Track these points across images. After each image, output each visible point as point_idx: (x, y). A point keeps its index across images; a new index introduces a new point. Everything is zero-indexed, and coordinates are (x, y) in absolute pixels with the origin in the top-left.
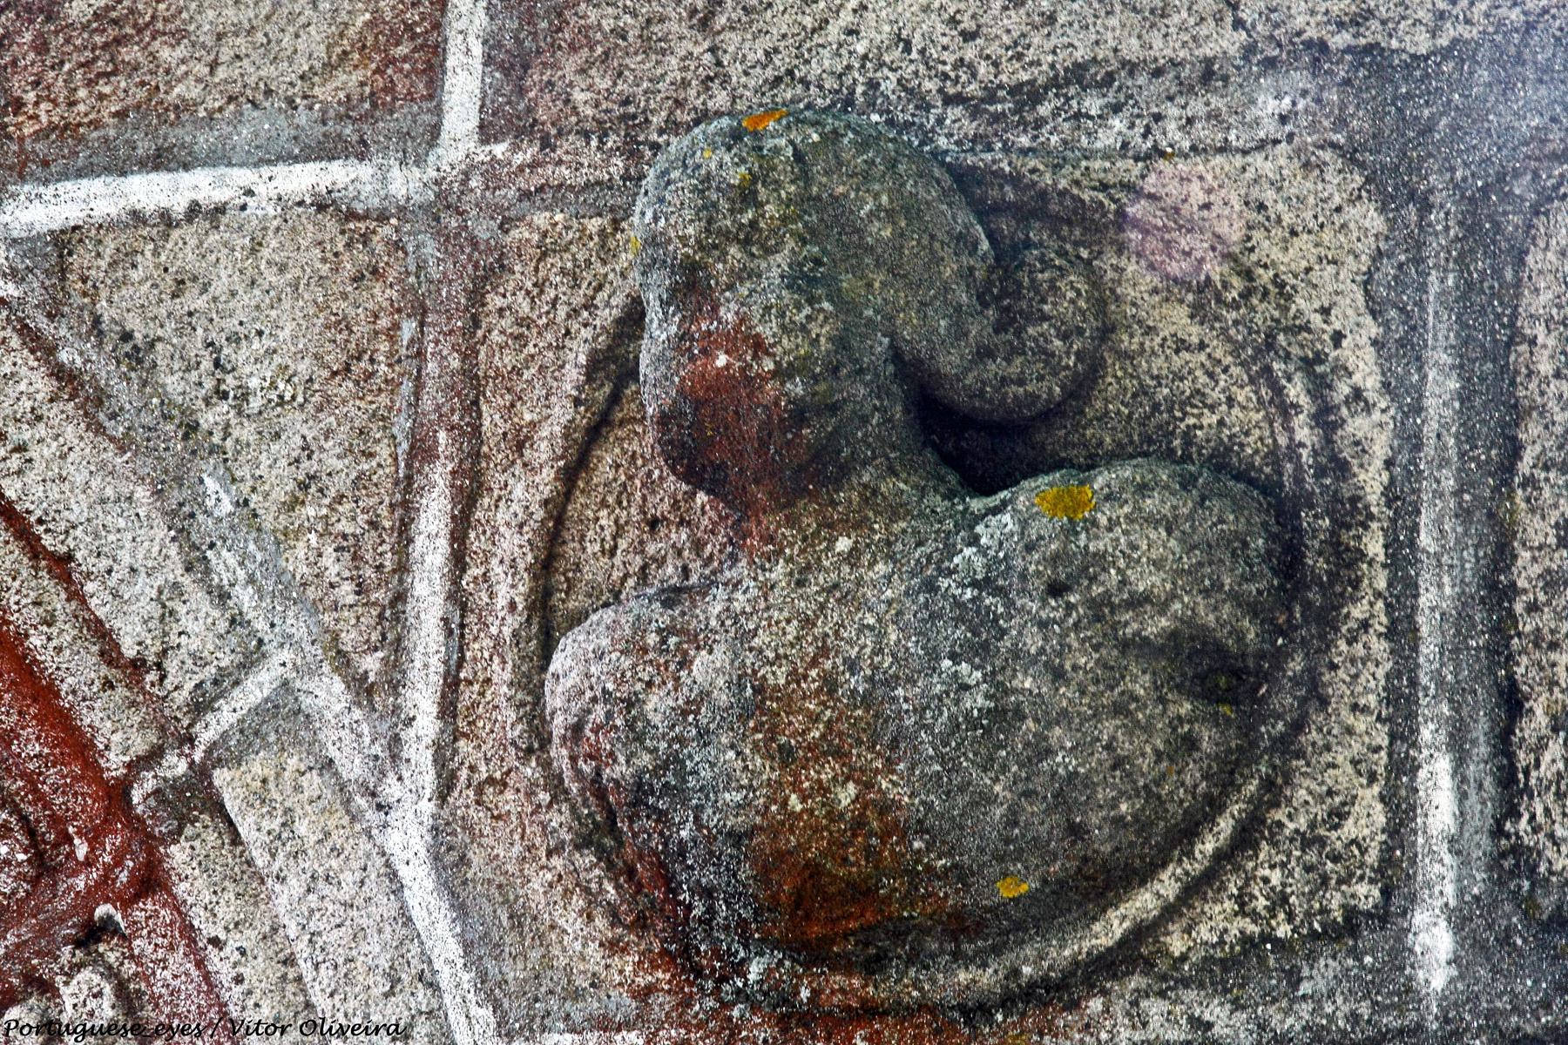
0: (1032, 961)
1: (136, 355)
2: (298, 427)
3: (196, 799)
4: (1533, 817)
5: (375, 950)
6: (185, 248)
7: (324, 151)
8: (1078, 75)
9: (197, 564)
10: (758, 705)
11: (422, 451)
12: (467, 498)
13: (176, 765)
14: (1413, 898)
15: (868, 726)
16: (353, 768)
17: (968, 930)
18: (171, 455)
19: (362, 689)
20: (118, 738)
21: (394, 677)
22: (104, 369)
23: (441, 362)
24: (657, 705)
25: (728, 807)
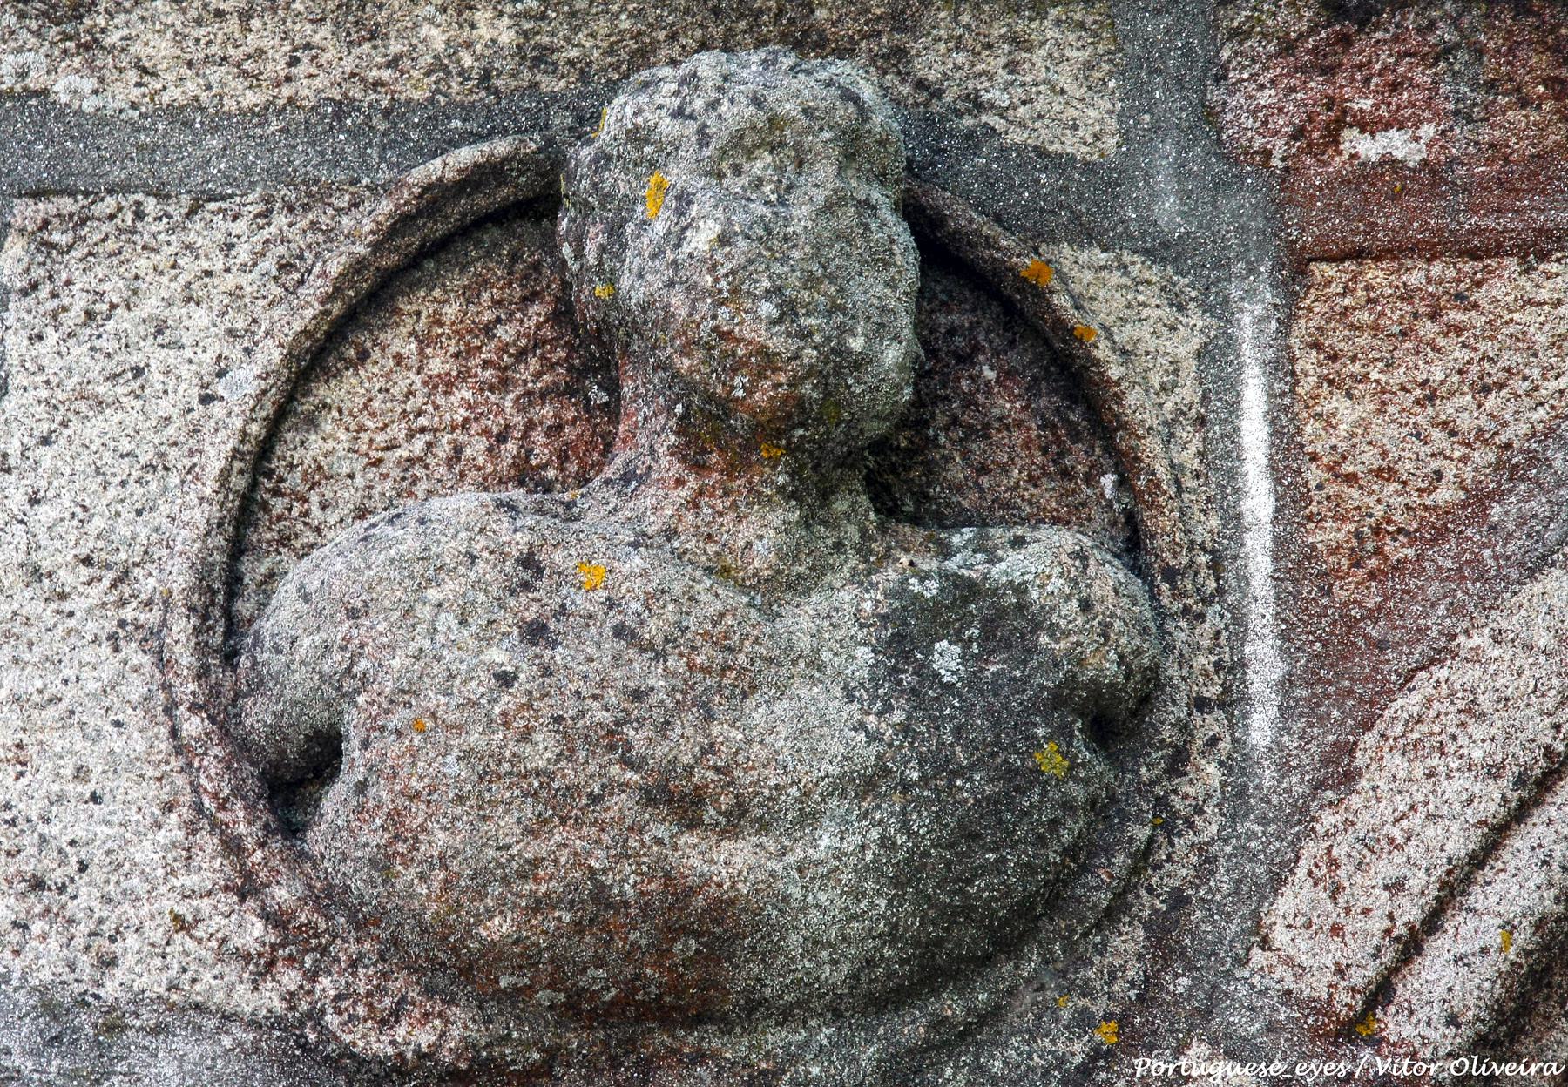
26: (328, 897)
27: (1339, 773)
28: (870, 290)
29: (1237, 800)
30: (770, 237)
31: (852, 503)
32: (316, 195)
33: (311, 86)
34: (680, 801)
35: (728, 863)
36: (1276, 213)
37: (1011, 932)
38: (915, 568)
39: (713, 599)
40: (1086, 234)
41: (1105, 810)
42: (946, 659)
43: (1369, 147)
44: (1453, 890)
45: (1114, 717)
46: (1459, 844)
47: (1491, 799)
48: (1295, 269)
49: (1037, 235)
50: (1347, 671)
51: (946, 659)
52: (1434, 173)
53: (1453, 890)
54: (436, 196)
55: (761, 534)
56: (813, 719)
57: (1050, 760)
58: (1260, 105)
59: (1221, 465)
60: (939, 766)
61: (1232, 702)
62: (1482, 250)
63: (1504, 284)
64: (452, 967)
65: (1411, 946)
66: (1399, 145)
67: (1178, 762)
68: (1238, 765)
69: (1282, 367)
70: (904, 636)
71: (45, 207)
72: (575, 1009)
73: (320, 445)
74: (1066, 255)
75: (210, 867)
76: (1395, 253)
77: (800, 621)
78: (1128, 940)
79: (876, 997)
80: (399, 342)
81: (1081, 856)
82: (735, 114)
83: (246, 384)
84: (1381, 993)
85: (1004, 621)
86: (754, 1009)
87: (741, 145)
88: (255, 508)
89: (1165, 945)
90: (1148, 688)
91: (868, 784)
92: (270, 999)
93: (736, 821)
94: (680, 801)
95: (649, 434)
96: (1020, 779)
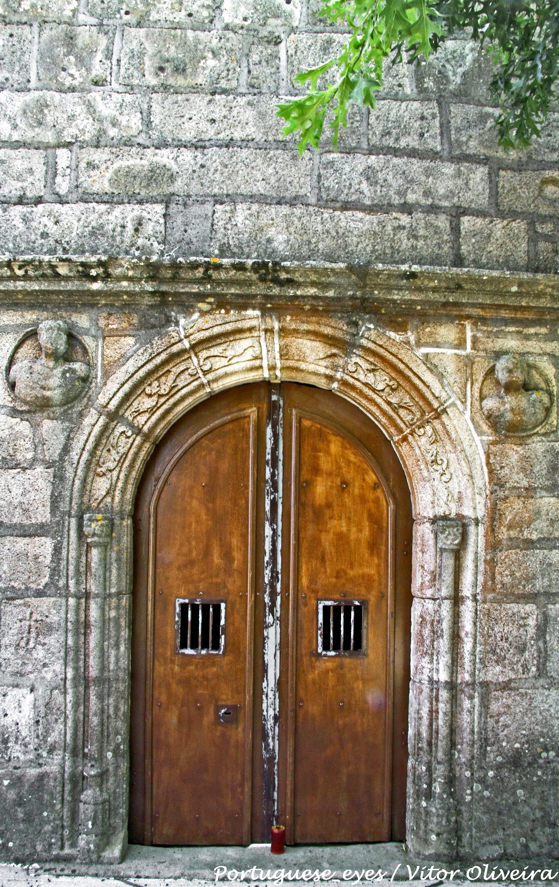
0: (529, 433)
1: (436, 367)
2: (454, 376)
3: (445, 411)
4: (308, 513)
5: (465, 427)
6: (441, 356)
7: (455, 348)
8: (528, 353)
9: (443, 388)
10: (512, 410)
11: (467, 380)
12: (472, 384)
13: (442, 408)
14: (129, 639)
15: (523, 412)
16: (461, 410)
17: (524, 430)
18: (441, 377)
19: (462, 402)
20: (436, 405)
21: (466, 402)
22: (432, 367)
23: (469, 371)
24: (502, 409)
25: (508, 419)
26: (16, 396)
27: (105, 384)
28: (60, 342)
29: (96, 387)
30: (50, 337)
31: (61, 361)
32: (18, 332)
33: (18, 322)
34: (43, 388)
35: (48, 393)
36: (102, 333)
37: (75, 399)
38: (66, 366)
39: (47, 370)
40: (86, 335)
41: (83, 388)
42: (68, 375)
43: (110, 326)
44: (115, 394)
45: (85, 380)
46: (115, 390)
47: (118, 386)
48: (104, 338)
49: (81, 335)
50: (107, 375)
51: (68, 375)
52: (117, 329)
53: (115, 394)
54: (27, 333)
55: (51, 364)
56: (55, 381)
57: (77, 384)
58: (102, 323)
59: (97, 356)
60: (66, 385)
61: (96, 378)
62: (121, 336)
63: (123, 339)
64: (26, 403)
65: (111, 399)
66: (114, 327)
67: (91, 383)
68: (96, 384)
69: (103, 347)
70: (64, 373)
71: (218, 261)
72: (37, 406)
73: (18, 355)
74: (85, 337)
75: (7, 393)
76: (113, 336)
77: (55, 372)
78: (86, 399)
79: (62, 405)
80: (25, 345)
81: (81, 392)
82: (48, 326)
83: (11, 350)
84: (108, 403)
85: (73, 371)
86: (52, 406)
87: (48, 329)
88: (12, 361)
89: (89, 400)
90: (88, 377)
91: (60, 386)
92: (12, 405)
93: (49, 389)
94: (43, 388)
95: (43, 356)
96: (74, 386)
